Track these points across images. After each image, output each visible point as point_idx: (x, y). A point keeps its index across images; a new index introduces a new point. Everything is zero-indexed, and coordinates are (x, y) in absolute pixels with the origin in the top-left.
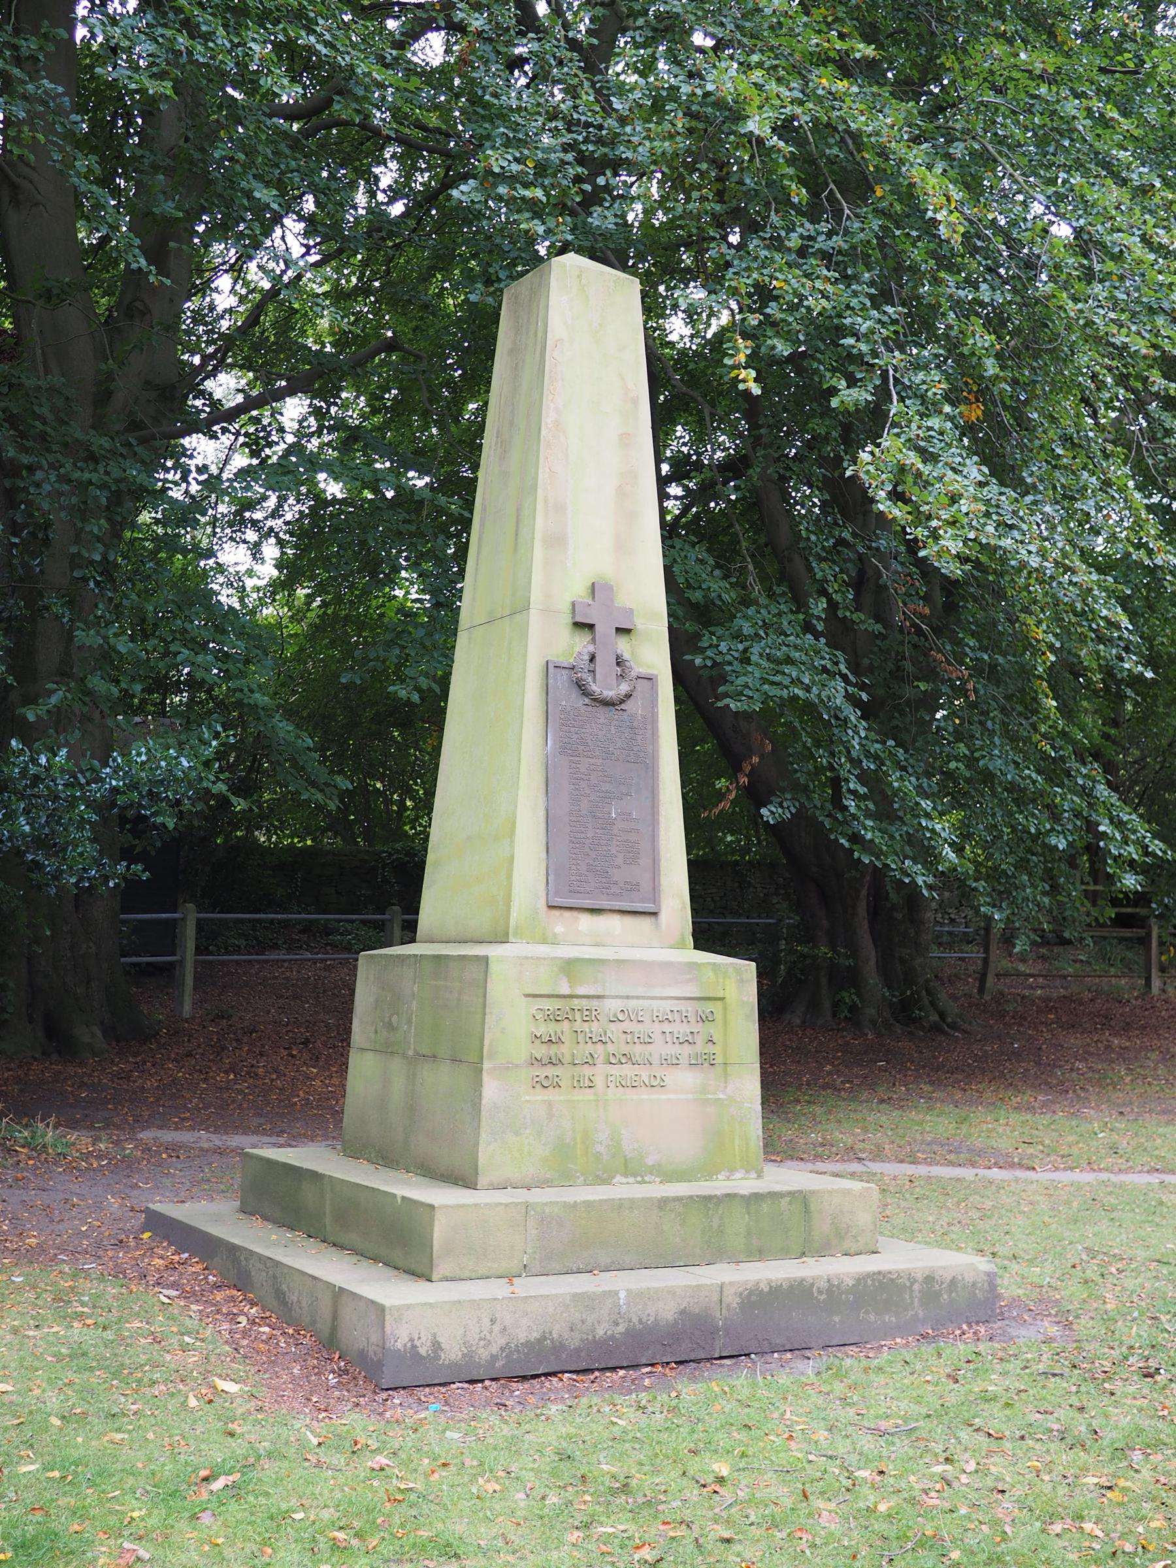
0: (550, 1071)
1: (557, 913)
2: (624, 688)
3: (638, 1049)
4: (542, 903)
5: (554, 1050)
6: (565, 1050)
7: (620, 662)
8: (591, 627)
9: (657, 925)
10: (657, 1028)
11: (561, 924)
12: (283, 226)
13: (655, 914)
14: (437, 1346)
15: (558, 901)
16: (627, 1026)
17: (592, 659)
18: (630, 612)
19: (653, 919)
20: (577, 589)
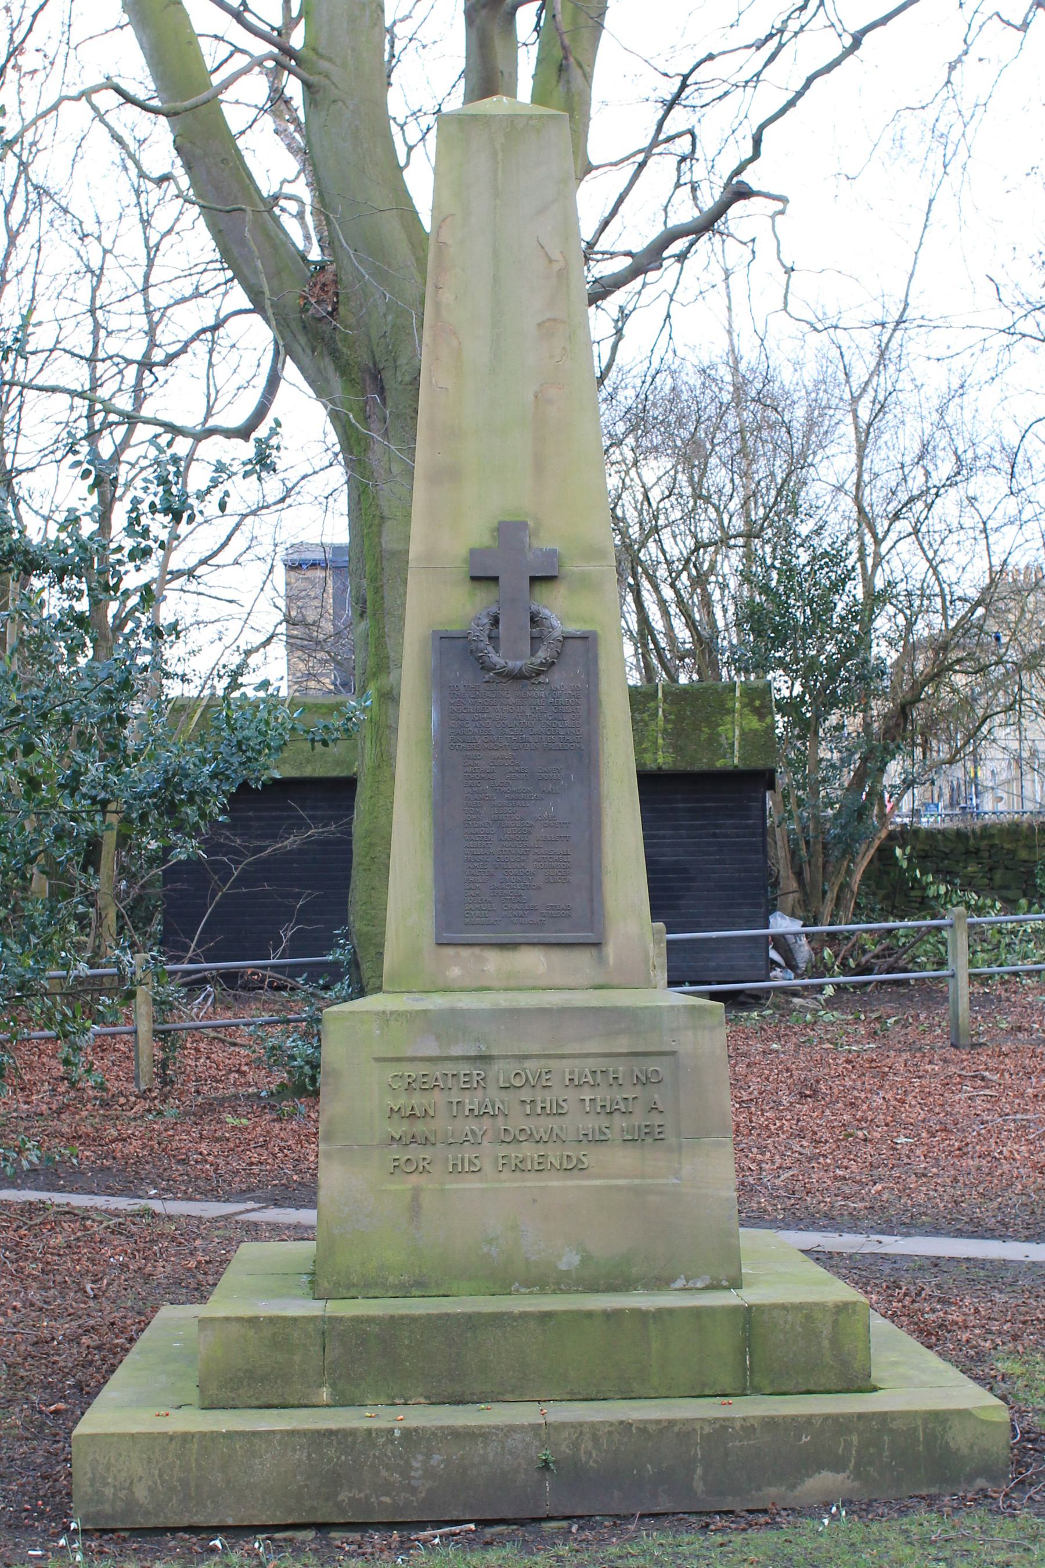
0: (417, 1153)
1: (450, 951)
2: (542, 654)
3: (543, 1125)
4: (427, 940)
5: (420, 1127)
6: (441, 1124)
7: (535, 619)
8: (495, 579)
9: (601, 960)
10: (571, 1095)
11: (458, 965)
12: (276, 198)
13: (597, 945)
14: (958, 1449)
15: (447, 936)
16: (526, 1095)
17: (496, 621)
18: (553, 554)
19: (594, 951)
20: (473, 532)
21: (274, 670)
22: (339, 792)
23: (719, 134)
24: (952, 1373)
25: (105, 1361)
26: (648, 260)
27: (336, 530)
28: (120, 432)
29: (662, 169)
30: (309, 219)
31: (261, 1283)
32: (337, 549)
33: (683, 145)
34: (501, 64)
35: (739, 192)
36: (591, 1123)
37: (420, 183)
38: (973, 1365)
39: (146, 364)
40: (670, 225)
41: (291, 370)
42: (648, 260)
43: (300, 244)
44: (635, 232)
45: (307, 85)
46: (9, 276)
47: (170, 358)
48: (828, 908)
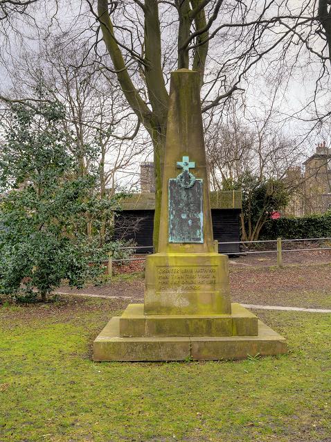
21: (138, 189)
22: (152, 212)
23: (232, 76)
24: (277, 334)
25: (100, 329)
26: (215, 103)
27: (151, 159)
28: (107, 138)
29: (218, 83)
30: (147, 94)
31: (133, 311)
32: (151, 163)
33: (223, 78)
34: (186, 62)
35: (235, 88)
36: (201, 280)
37: (168, 87)
38: (280, 332)
39: (112, 124)
40: (114, 29)
41: (142, 127)
42: (215, 103)
43: (143, 99)
44: (212, 97)
45: (145, 67)
46: (328, 119)
47: (117, 123)
48: (252, 238)
